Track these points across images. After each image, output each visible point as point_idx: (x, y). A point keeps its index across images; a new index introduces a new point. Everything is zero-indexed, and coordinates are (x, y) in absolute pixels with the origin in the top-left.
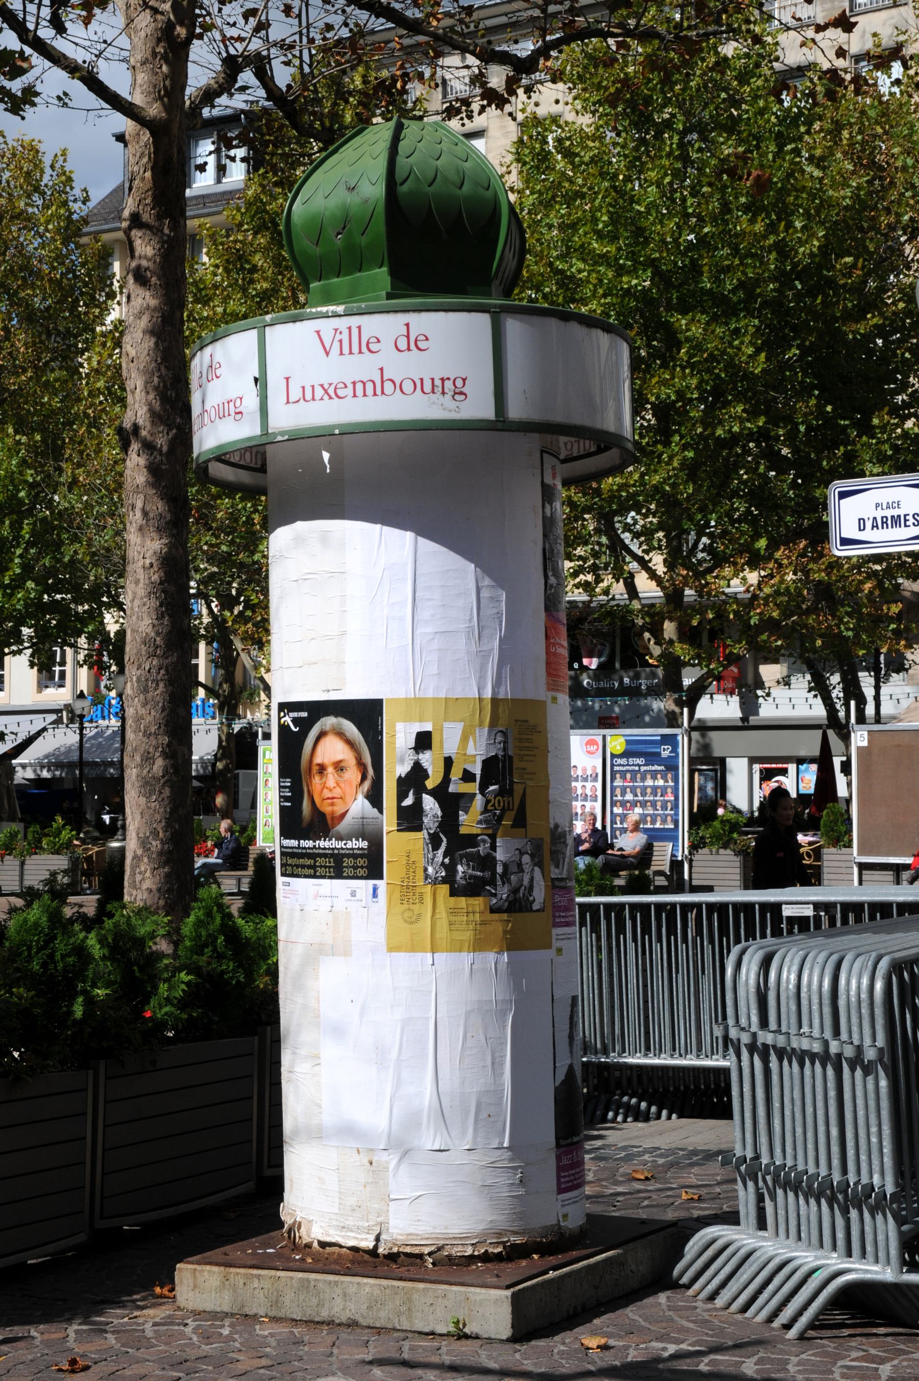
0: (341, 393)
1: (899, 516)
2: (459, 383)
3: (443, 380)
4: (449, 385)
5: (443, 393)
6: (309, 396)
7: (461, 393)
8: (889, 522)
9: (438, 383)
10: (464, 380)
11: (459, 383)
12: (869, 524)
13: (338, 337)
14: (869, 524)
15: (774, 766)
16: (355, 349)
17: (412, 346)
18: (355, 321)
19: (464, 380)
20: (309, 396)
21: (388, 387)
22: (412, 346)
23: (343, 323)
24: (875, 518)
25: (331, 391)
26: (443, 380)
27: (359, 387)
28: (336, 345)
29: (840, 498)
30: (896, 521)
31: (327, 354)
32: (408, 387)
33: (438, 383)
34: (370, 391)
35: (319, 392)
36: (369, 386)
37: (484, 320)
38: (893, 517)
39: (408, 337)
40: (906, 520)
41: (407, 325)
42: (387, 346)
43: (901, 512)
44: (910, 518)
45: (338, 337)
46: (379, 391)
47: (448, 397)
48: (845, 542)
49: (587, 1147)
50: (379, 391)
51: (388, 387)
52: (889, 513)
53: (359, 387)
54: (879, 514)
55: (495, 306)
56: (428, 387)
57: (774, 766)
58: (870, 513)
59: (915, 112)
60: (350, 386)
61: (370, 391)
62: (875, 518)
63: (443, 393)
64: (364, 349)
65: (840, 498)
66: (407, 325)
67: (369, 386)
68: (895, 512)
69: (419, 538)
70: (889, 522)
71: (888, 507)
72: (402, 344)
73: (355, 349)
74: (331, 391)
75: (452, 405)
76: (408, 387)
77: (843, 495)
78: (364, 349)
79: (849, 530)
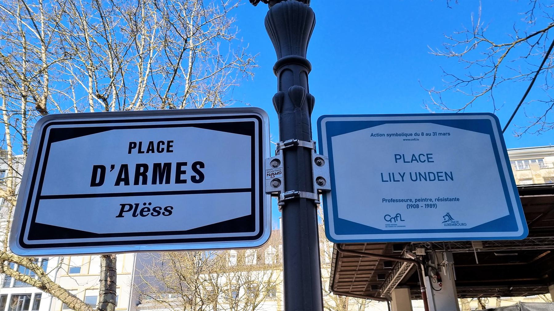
1: (168, 166)
8: (150, 174)
12: (111, 176)
14: (111, 176)
15: (506, 280)
24: (124, 167)
29: (51, 141)
37: (386, 302)
38: (157, 166)
40: (179, 172)
43: (172, 159)
44: (188, 169)
49: (381, 251)
52: (151, 159)
54: (133, 160)
57: (506, 280)
62: (124, 167)
65: (51, 141)
68: (162, 158)
69: (546, 295)
70: (150, 174)
71: (151, 149)
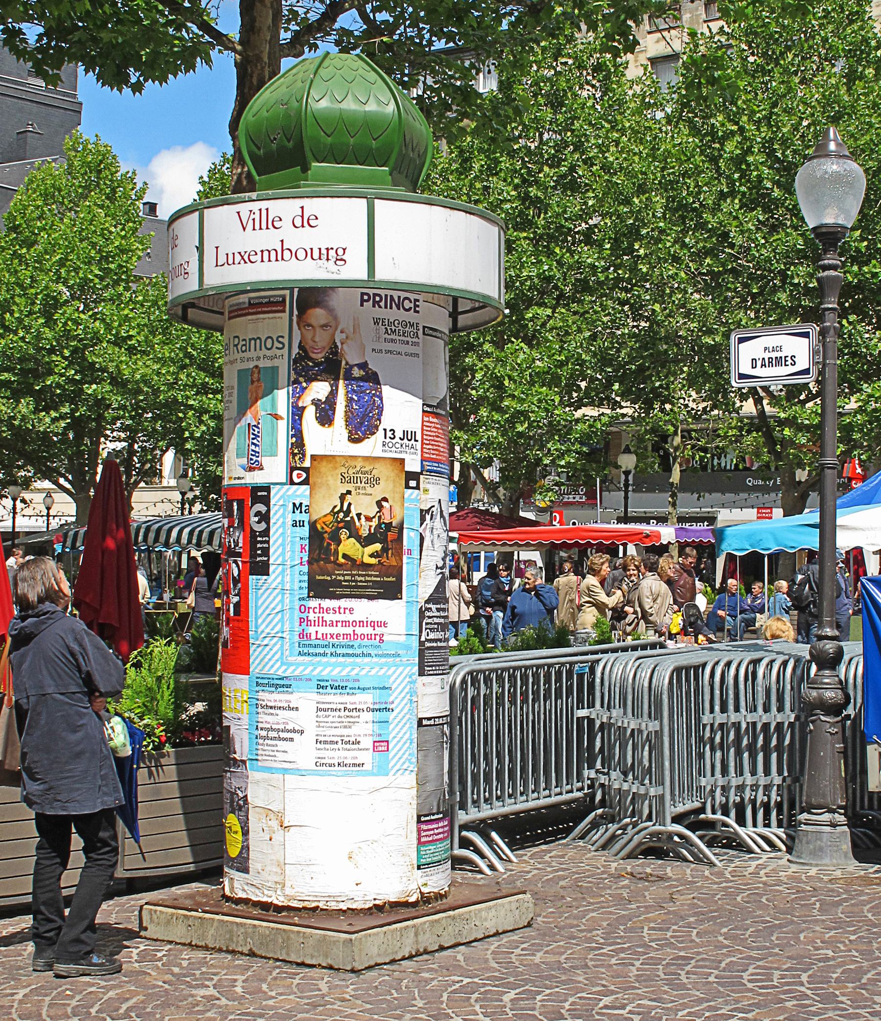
0: (253, 258)
2: (340, 252)
3: (327, 249)
4: (332, 253)
5: (328, 259)
6: (231, 261)
7: (342, 260)
9: (324, 252)
10: (344, 250)
11: (340, 252)
12: (759, 363)
13: (252, 216)
14: (759, 363)
16: (264, 226)
17: (305, 224)
18: (264, 205)
19: (344, 250)
20: (231, 261)
21: (287, 254)
22: (305, 224)
23: (255, 206)
25: (246, 258)
26: (327, 249)
27: (266, 254)
28: (251, 222)
30: (779, 361)
31: (244, 229)
32: (301, 254)
33: (324, 252)
34: (273, 257)
35: (238, 258)
36: (273, 253)
39: (302, 217)
41: (302, 208)
42: (286, 223)
43: (783, 354)
44: (788, 359)
45: (252, 216)
46: (279, 258)
47: (331, 262)
48: (742, 376)
50: (279, 258)
51: (287, 254)
52: (774, 355)
53: (266, 254)
54: (767, 355)
55: (371, 194)
56: (316, 255)
58: (760, 354)
59: (877, 48)
60: (259, 254)
61: (273, 257)
63: (328, 259)
64: (270, 226)
66: (302, 208)
67: (273, 253)
68: (778, 354)
72: (298, 222)
73: (264, 226)
74: (246, 258)
75: (334, 268)
76: (301, 254)
77: (741, 340)
78: (270, 226)
79: (746, 369)
